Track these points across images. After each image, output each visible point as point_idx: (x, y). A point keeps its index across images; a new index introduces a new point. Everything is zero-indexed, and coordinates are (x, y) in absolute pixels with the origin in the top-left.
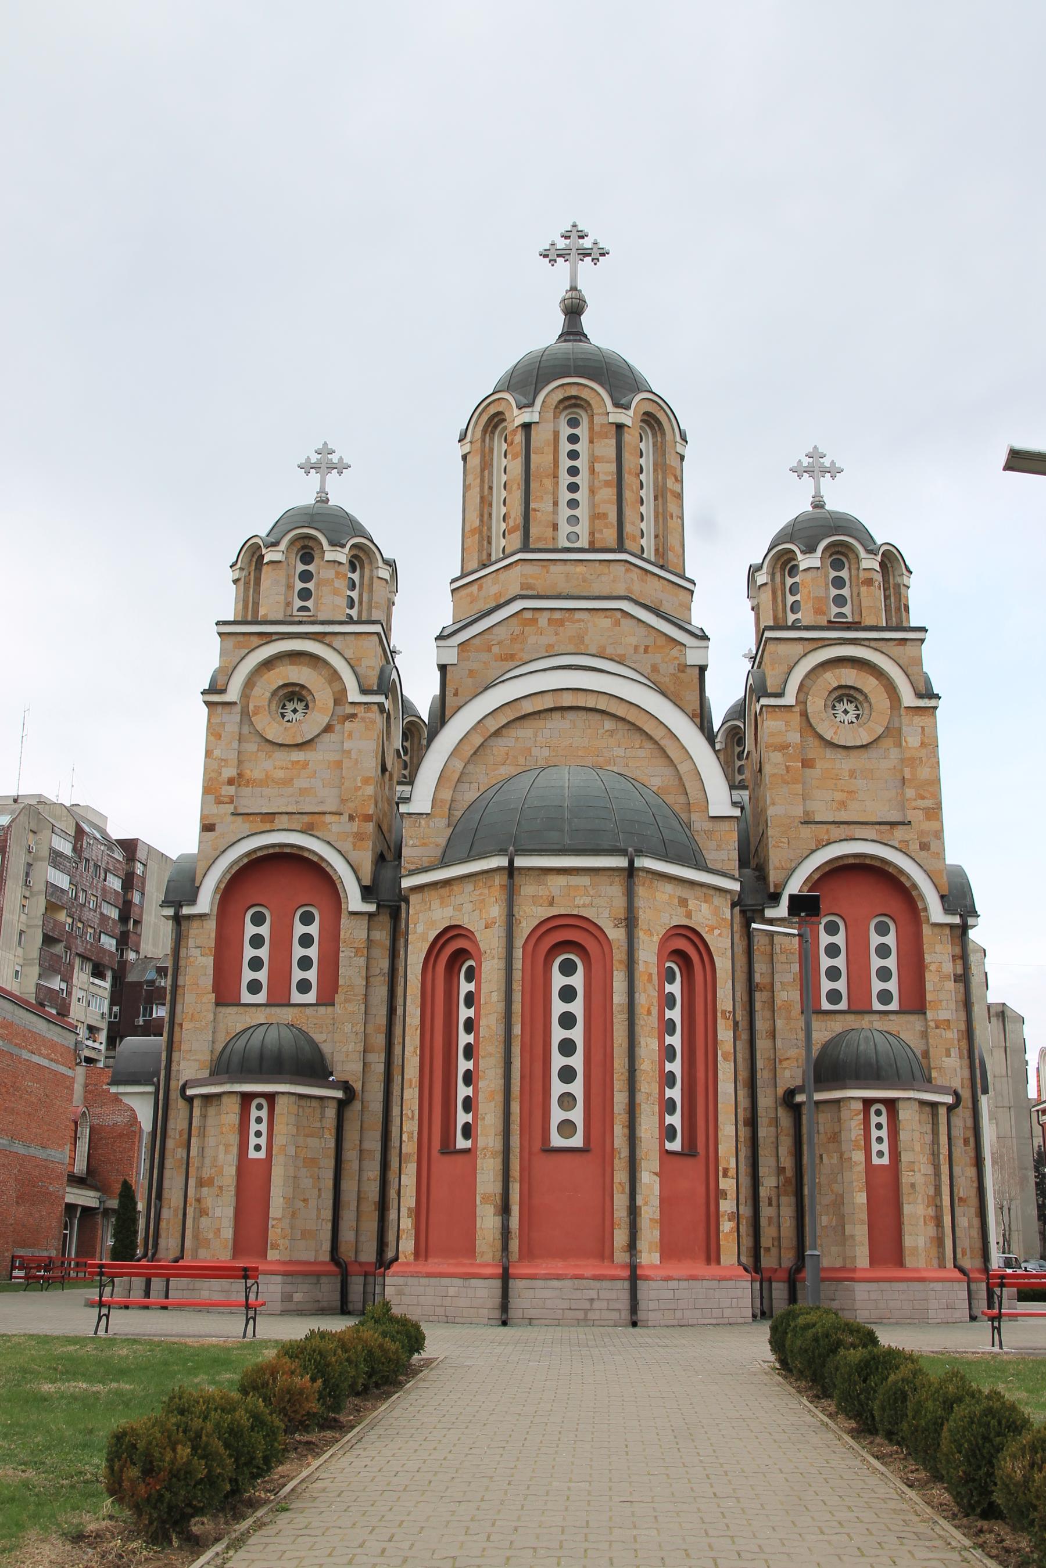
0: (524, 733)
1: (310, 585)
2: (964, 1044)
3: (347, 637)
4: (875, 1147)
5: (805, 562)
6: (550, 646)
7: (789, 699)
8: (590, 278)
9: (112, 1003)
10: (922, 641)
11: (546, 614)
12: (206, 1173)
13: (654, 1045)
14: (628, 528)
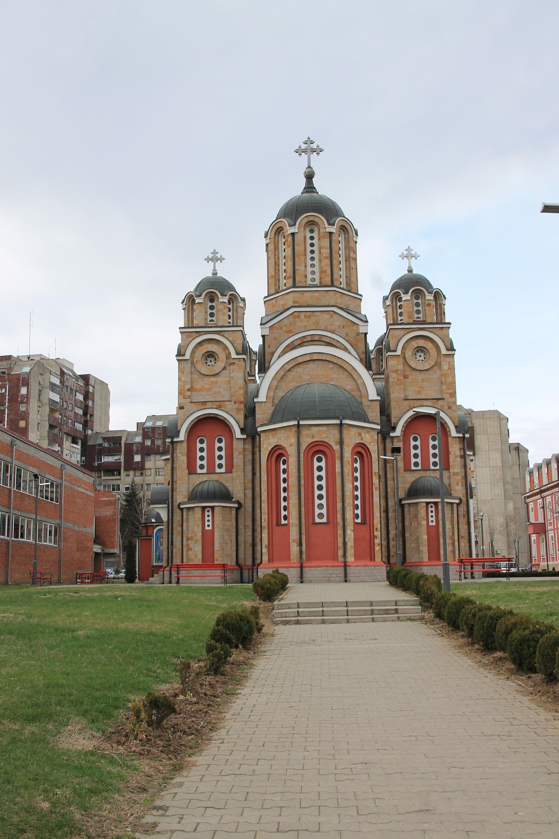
0: (299, 370)
1: (214, 311)
2: (464, 481)
3: (230, 332)
4: (430, 519)
5: (405, 297)
6: (306, 327)
7: (399, 352)
8: (316, 162)
9: (82, 456)
10: (449, 328)
11: (304, 314)
12: (190, 535)
13: (351, 486)
14: (335, 276)
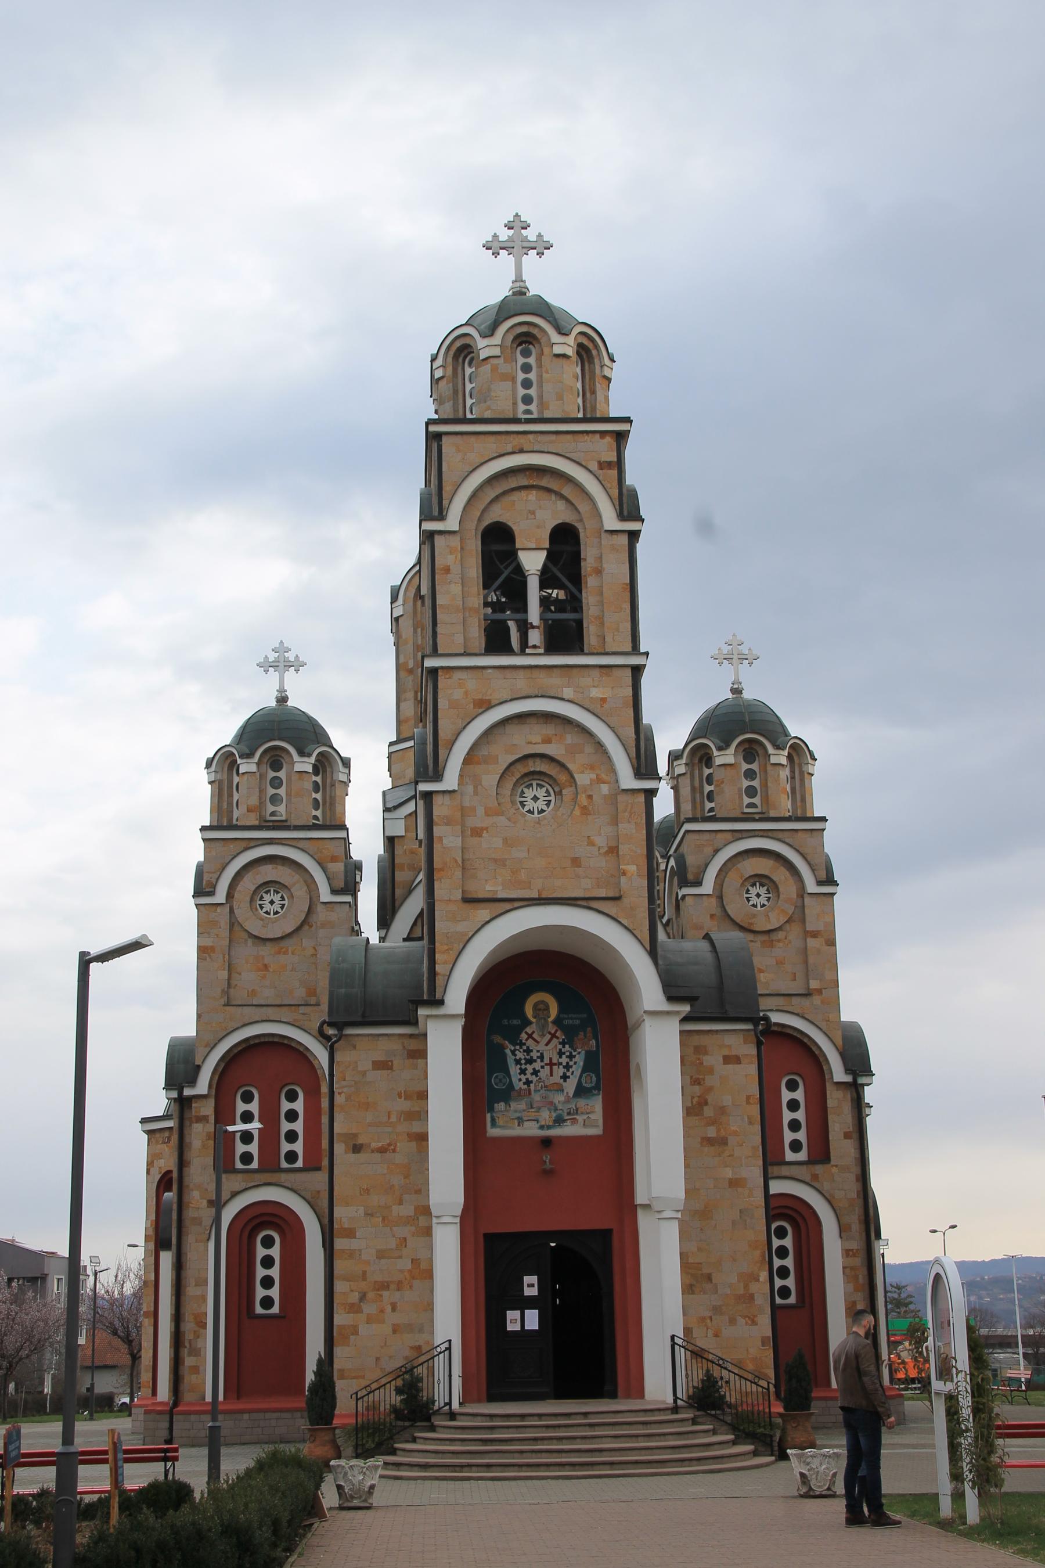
7: (708, 886)
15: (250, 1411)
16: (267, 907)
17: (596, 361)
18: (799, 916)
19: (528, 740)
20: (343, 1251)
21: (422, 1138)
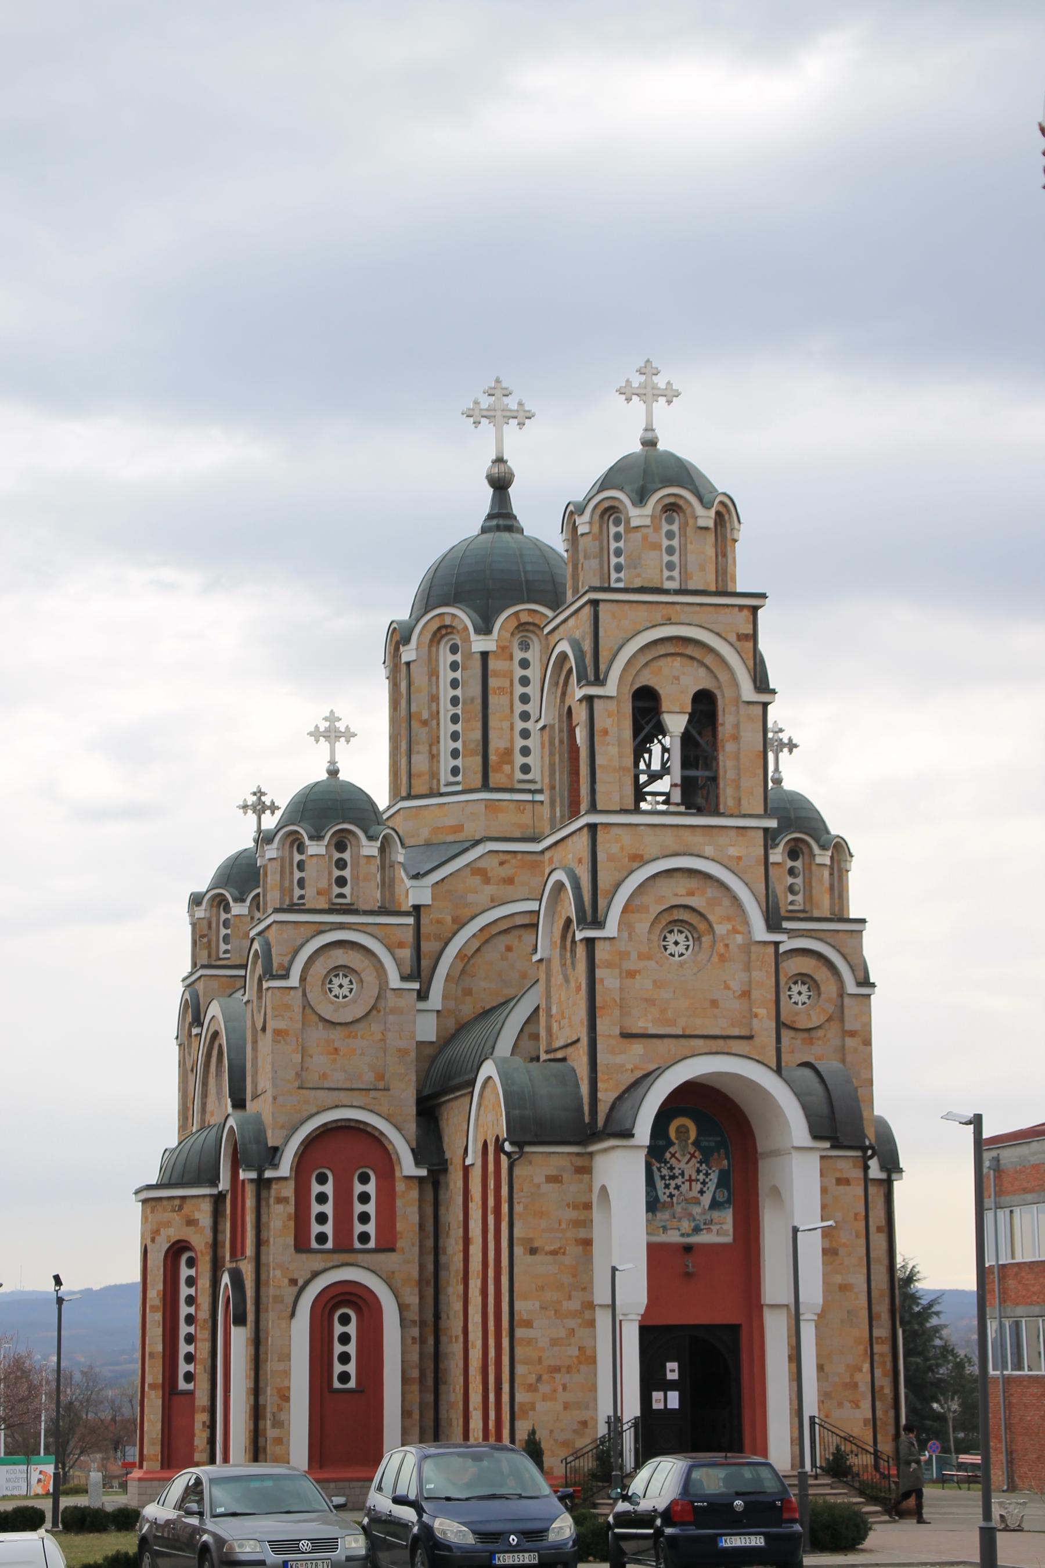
1: (337, 873)
7: (294, 980)
15: (335, 1480)
16: (336, 991)
17: (728, 525)
18: (839, 1015)
19: (675, 892)
20: (523, 1339)
21: (588, 1243)
